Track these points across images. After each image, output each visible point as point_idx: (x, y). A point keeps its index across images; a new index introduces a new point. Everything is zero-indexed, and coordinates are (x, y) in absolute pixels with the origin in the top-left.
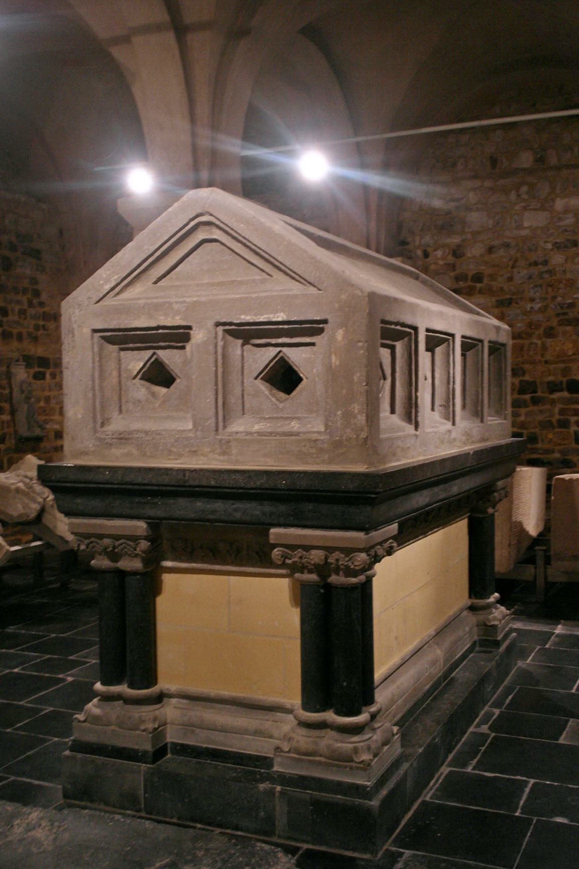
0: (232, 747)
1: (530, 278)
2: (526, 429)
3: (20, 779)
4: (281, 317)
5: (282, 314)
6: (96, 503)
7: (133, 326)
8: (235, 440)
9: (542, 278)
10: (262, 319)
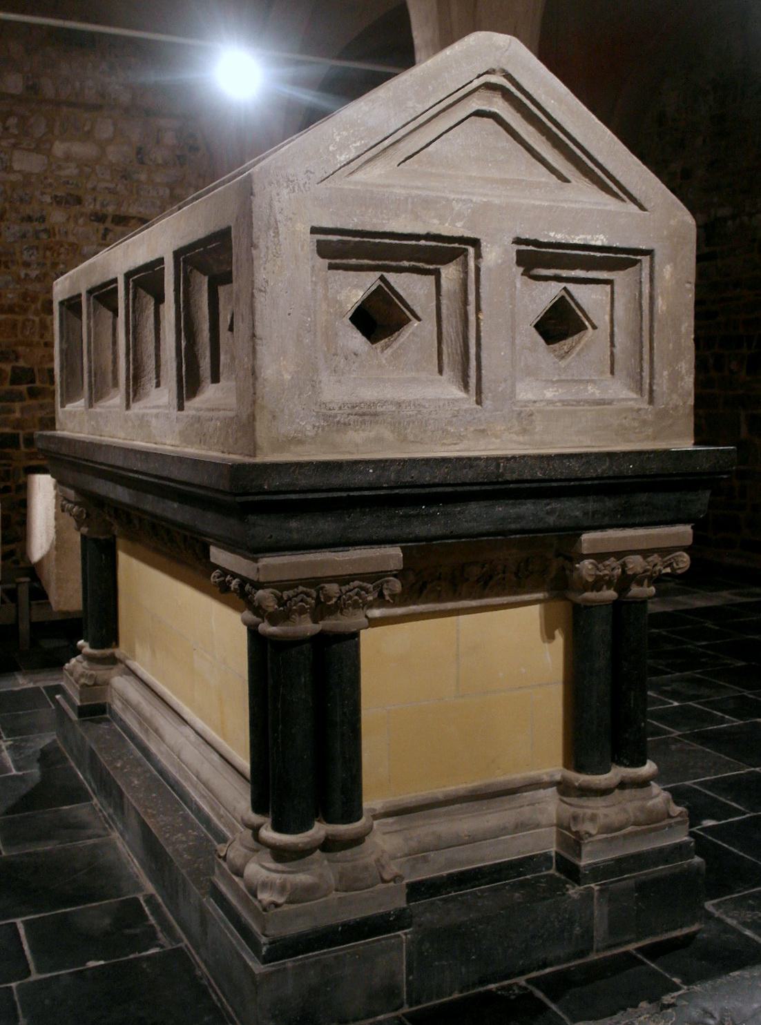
0: (483, 860)
1: (24, 236)
2: (23, 429)
3: (661, 971)
4: (599, 240)
5: (602, 237)
6: (326, 526)
7: (387, 229)
8: (539, 412)
9: (38, 238)
10: (578, 239)
